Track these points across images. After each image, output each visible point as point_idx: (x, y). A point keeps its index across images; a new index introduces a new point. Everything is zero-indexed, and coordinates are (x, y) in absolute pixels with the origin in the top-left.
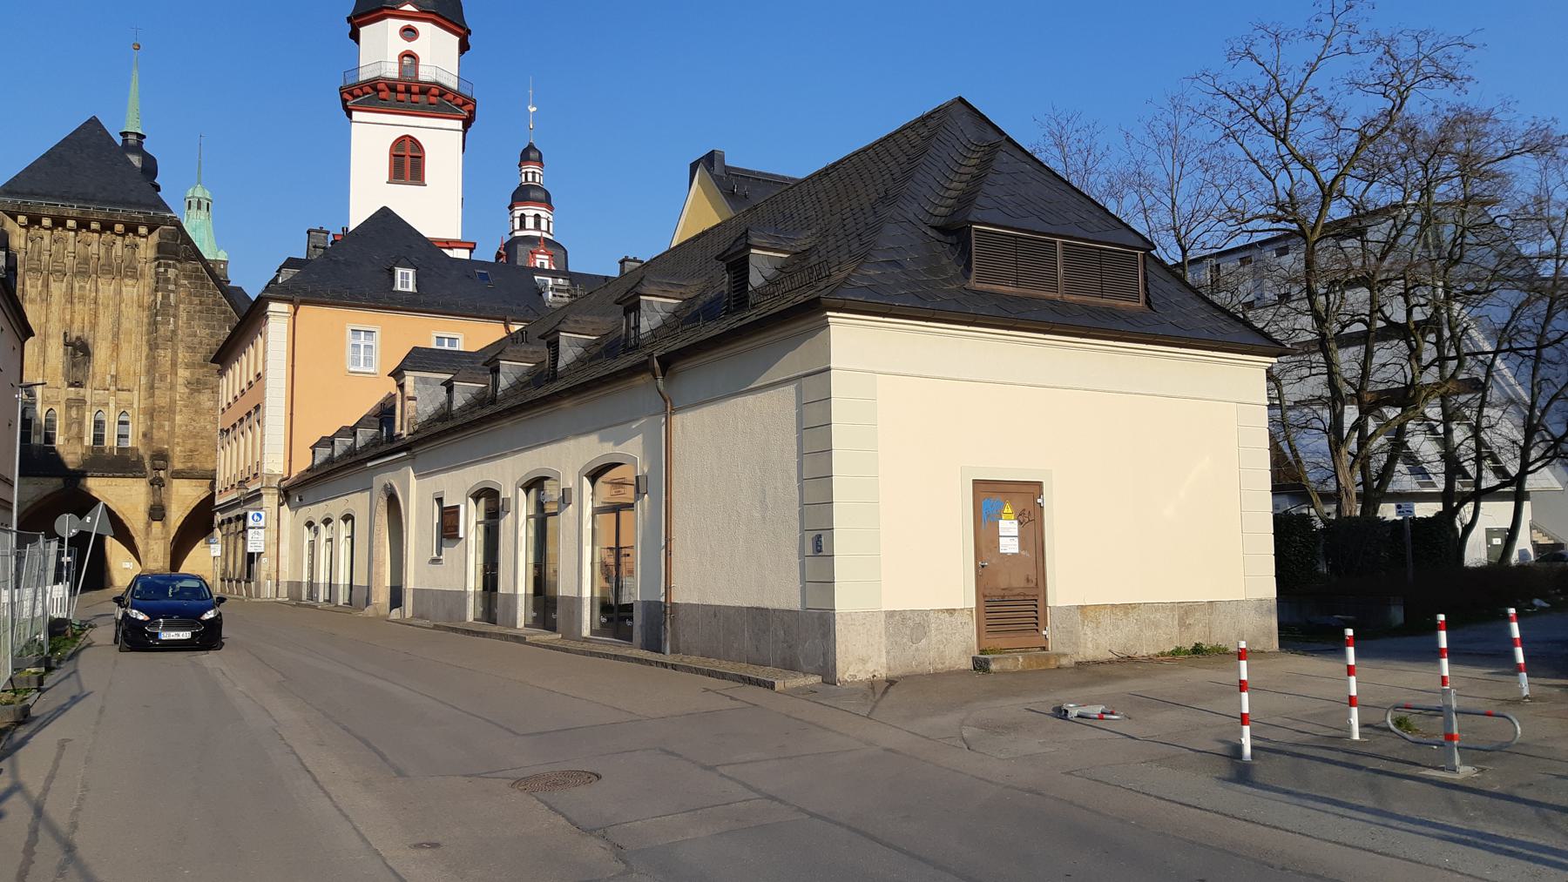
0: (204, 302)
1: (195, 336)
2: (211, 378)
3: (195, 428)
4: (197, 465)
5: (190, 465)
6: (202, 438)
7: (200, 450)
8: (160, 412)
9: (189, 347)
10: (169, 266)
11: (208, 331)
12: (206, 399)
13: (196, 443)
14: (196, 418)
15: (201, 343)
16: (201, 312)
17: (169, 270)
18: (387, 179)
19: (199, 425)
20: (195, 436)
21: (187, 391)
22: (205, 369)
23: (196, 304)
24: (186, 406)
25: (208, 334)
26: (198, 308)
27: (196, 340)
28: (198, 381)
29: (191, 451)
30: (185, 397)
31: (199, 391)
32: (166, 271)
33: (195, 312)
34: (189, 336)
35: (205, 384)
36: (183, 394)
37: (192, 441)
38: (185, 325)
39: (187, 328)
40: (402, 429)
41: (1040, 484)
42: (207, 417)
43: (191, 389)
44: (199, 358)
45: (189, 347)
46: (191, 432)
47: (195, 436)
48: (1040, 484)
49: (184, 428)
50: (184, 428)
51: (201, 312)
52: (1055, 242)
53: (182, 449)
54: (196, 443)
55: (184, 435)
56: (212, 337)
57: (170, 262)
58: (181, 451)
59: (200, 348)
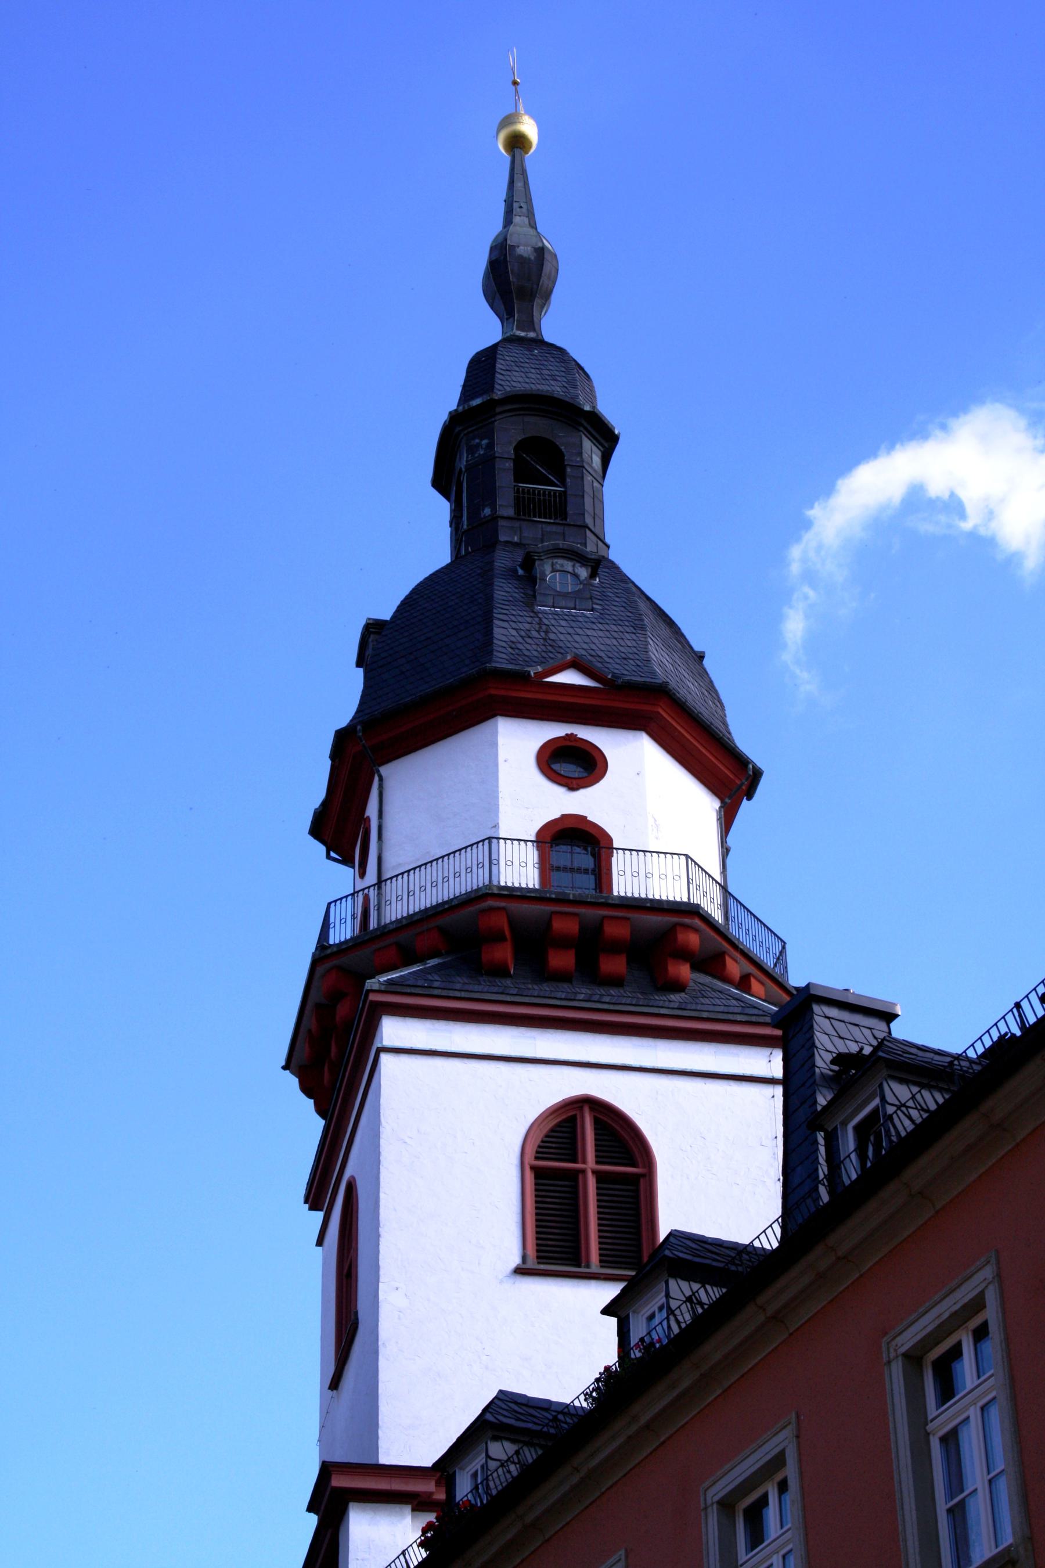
18: (515, 1260)
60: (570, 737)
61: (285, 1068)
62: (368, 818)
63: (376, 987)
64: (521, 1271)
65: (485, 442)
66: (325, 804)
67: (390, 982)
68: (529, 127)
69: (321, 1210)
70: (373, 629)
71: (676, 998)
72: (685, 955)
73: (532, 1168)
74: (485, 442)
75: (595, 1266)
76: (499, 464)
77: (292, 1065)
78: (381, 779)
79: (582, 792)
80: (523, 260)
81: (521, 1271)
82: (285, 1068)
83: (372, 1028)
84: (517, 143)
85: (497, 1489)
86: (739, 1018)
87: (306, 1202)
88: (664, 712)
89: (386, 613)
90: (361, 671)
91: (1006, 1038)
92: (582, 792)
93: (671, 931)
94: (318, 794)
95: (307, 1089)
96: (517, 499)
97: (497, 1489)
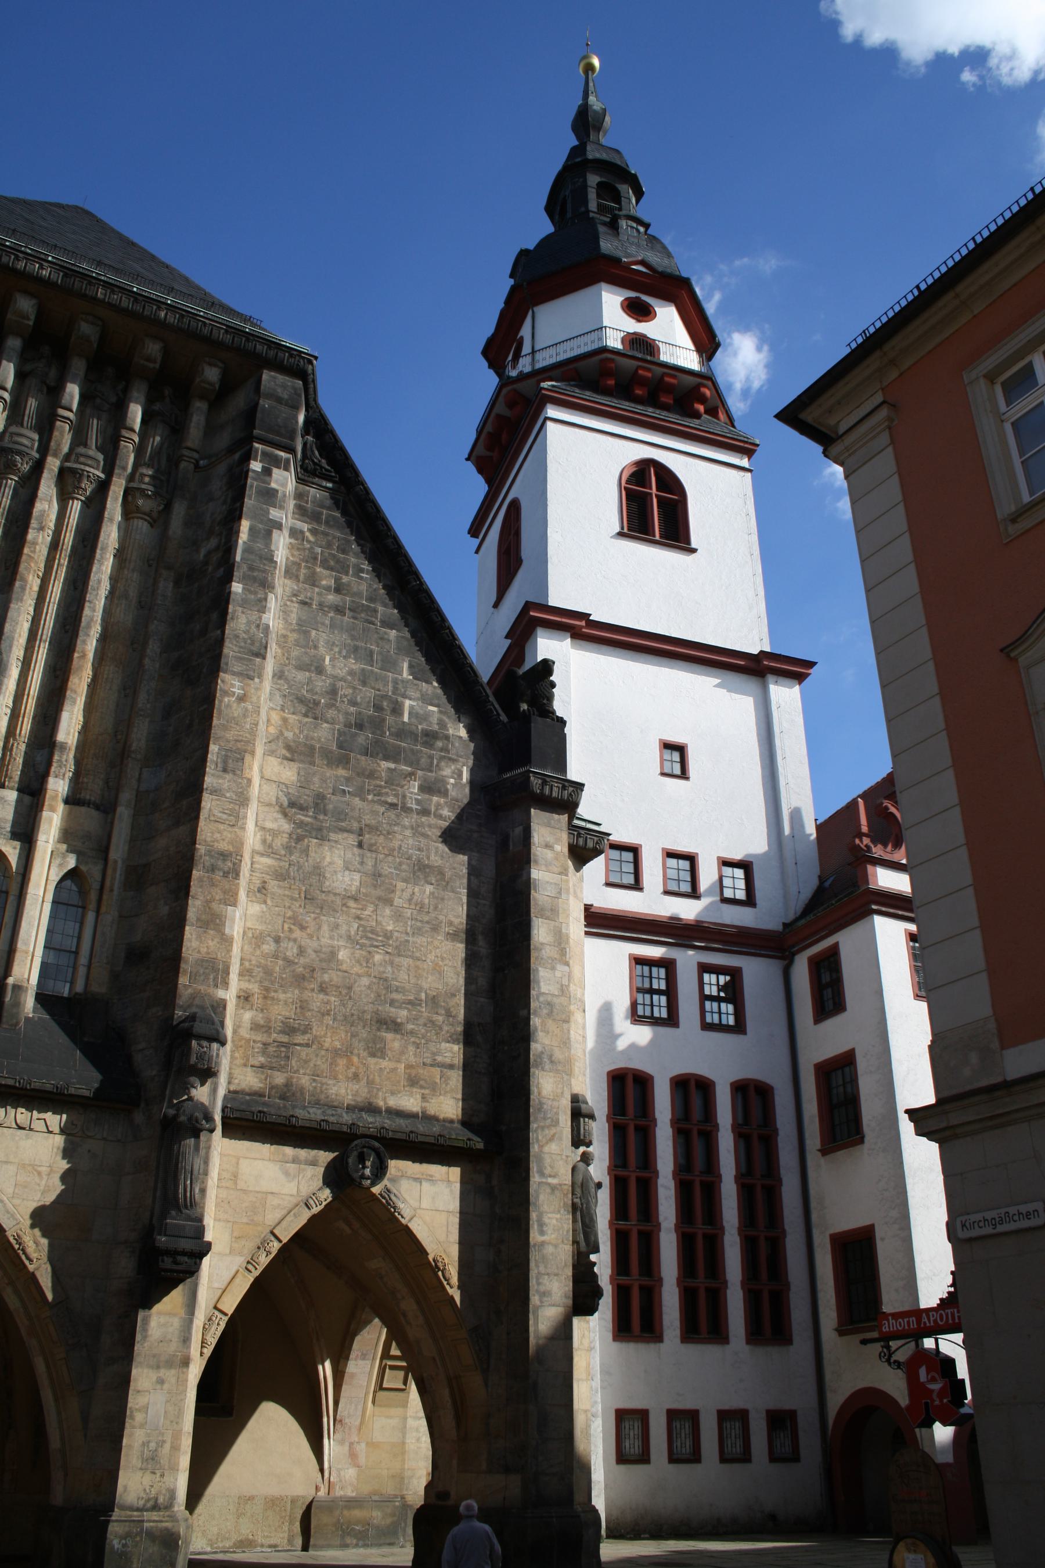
0: (349, 584)
1: (320, 670)
2: (357, 801)
3: (302, 951)
4: (305, 1081)
5: (279, 1079)
6: (323, 989)
7: (317, 1030)
8: (213, 869)
9: (301, 700)
10: (277, 462)
11: (353, 664)
12: (340, 862)
13: (303, 1006)
14: (309, 918)
15: (333, 692)
16: (339, 610)
17: (276, 472)
18: (617, 529)
19: (315, 944)
20: (300, 980)
21: (286, 826)
22: (341, 772)
23: (328, 589)
24: (281, 876)
25: (351, 673)
26: (331, 598)
27: (321, 684)
28: (319, 803)
29: (289, 1030)
30: (279, 843)
31: (320, 834)
32: (267, 472)
33: (321, 605)
34: (300, 668)
35: (340, 815)
36: (275, 833)
37: (293, 994)
38: (295, 635)
39: (297, 643)
40: (68, 734)
41: (583, 785)
42: (341, 919)
43: (301, 825)
44: (324, 734)
45: (301, 700)
46: (289, 962)
47: (300, 980)
48: (583, 785)
49: (269, 947)
50: (269, 947)
51: (339, 610)
52: (629, 530)
53: (260, 1019)
54: (303, 1006)
55: (268, 972)
56: (364, 683)
57: (282, 454)
58: (255, 1027)
59: (330, 706)
60: (637, 298)
61: (467, 459)
62: (522, 338)
63: (546, 387)
64: (621, 534)
65: (581, 180)
66: (493, 335)
67: (553, 386)
68: (596, 62)
69: (477, 537)
70: (523, 253)
71: (697, 421)
72: (703, 400)
73: (625, 488)
74: (581, 180)
75: (657, 537)
76: (589, 189)
77: (473, 458)
78: (533, 312)
79: (643, 324)
80: (595, 112)
81: (621, 534)
82: (467, 459)
83: (541, 408)
84: (590, 67)
85: (996, 223)
86: (728, 435)
87: (469, 533)
88: (684, 295)
89: (531, 246)
90: (512, 282)
91: (50, 1297)
92: (643, 324)
93: (699, 386)
94: (489, 329)
95: (480, 471)
96: (598, 205)
97: (996, 223)
